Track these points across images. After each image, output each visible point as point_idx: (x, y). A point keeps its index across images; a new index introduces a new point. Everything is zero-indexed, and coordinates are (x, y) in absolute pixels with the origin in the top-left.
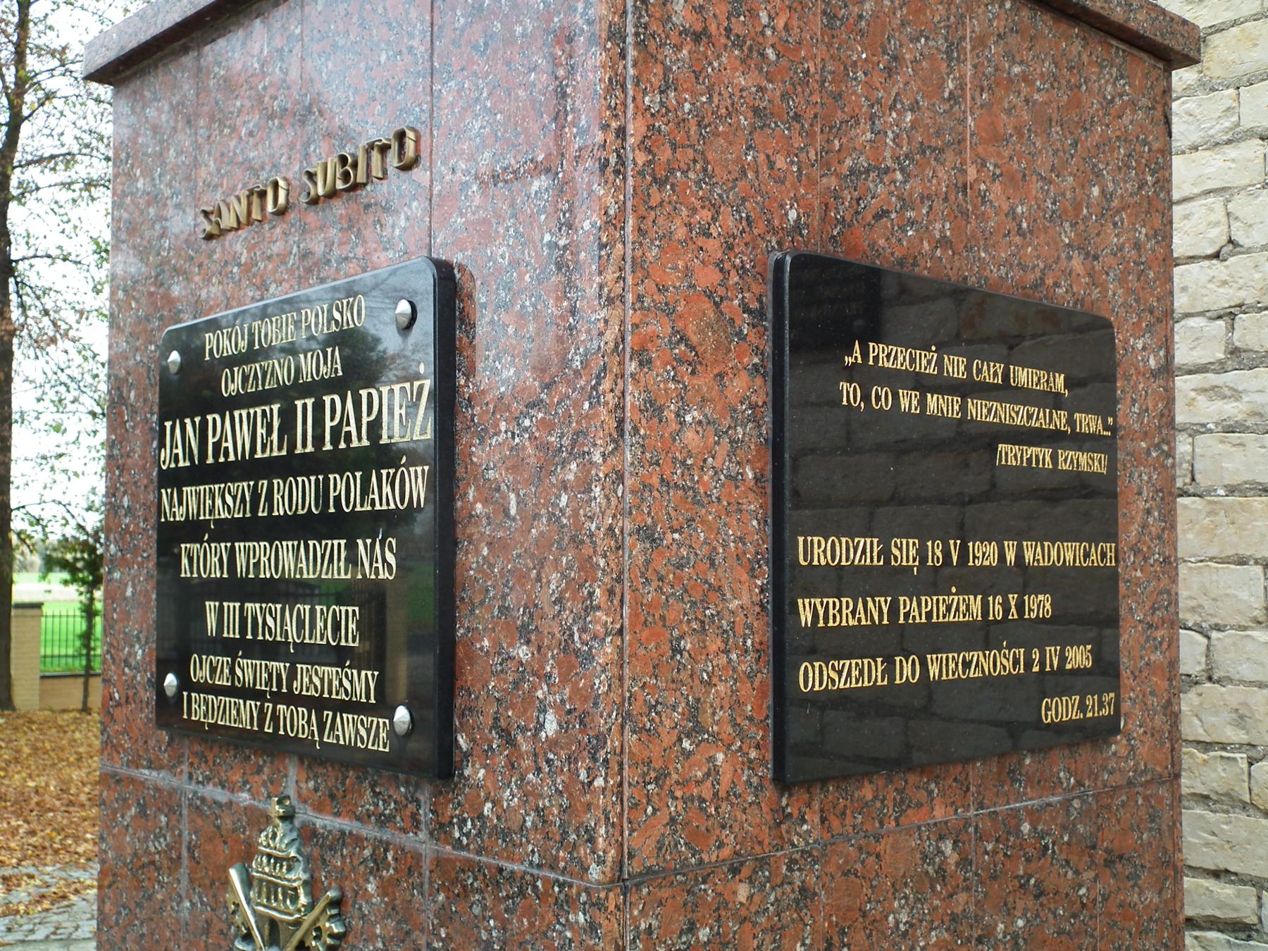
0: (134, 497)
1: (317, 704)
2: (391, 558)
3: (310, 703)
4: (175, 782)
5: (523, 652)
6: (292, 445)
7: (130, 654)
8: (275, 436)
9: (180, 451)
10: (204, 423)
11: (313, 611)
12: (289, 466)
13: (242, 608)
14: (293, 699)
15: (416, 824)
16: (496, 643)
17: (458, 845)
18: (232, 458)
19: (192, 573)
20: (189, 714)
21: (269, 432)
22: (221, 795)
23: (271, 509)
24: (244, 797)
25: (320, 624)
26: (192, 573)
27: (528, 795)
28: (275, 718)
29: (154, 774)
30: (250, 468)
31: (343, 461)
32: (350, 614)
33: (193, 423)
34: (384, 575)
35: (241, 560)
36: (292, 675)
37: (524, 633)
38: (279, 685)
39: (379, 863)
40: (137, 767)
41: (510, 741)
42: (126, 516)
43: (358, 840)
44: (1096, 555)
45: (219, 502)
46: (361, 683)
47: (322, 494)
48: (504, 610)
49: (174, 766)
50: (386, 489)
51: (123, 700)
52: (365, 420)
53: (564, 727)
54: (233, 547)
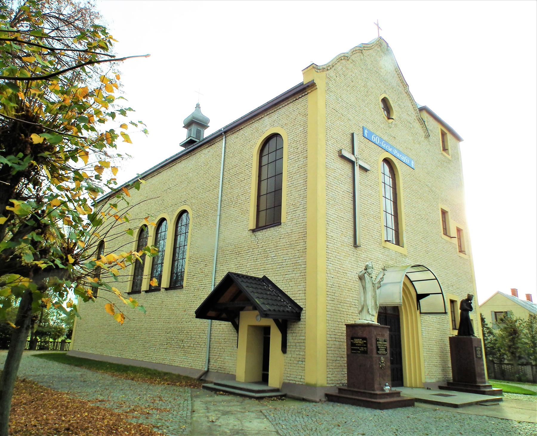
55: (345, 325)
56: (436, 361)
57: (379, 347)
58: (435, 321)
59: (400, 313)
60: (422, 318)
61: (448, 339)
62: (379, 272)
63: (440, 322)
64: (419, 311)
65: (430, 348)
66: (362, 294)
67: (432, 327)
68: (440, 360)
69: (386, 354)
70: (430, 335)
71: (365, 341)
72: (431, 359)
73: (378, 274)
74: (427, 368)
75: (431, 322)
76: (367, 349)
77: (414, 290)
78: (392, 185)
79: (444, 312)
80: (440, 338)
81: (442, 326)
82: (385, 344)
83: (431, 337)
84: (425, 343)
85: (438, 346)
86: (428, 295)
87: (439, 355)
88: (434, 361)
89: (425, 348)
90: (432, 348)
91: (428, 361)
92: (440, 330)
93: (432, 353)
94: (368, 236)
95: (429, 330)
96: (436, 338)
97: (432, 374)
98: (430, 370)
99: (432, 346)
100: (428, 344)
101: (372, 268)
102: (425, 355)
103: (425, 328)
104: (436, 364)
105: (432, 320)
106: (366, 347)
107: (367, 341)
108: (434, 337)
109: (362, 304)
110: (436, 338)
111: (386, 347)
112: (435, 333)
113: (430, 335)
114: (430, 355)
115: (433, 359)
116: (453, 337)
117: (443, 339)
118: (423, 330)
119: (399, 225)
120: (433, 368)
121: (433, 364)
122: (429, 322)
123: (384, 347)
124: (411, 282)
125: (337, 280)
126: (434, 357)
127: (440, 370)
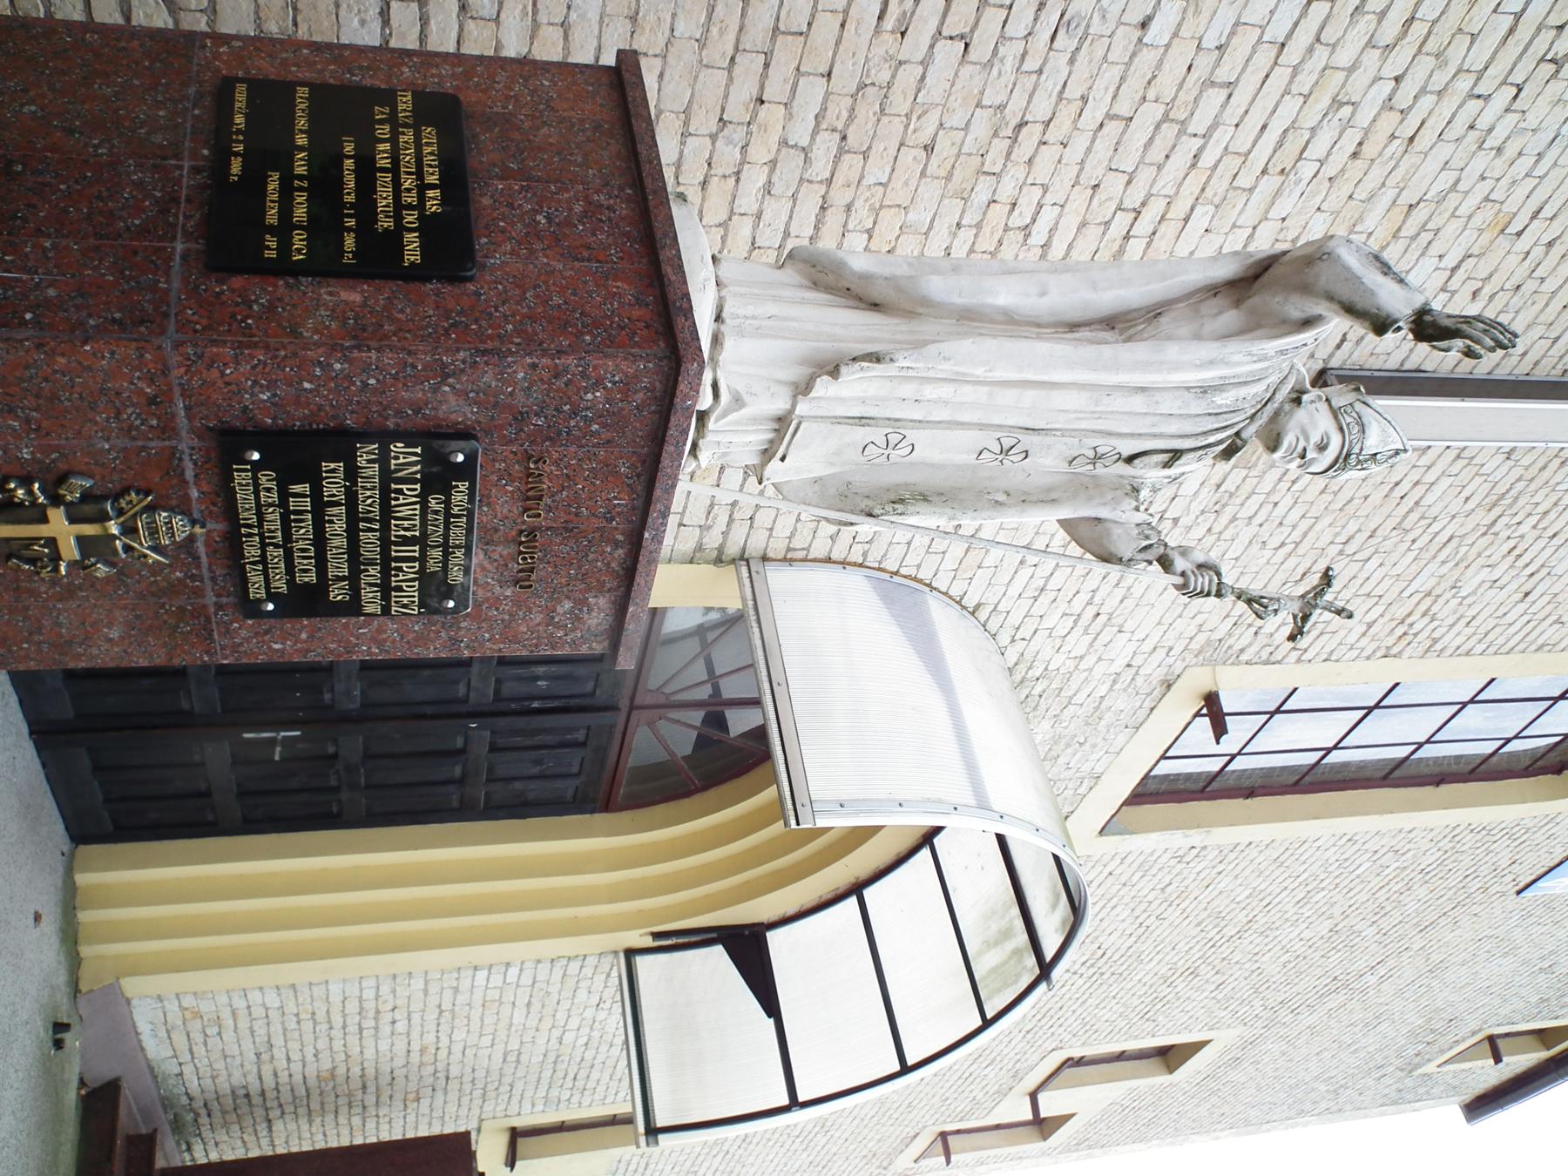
0: (375, 391)
1: (263, 560)
2: (339, 598)
3: (263, 555)
4: (184, 434)
5: (304, 636)
6: (396, 544)
7: (262, 386)
8: (402, 533)
9: (401, 461)
10: (415, 481)
11: (310, 558)
12: (385, 543)
13: (307, 511)
14: (263, 546)
15: (218, 596)
16: (306, 626)
17: (216, 614)
18: (393, 503)
19: (326, 472)
20: (238, 470)
21: (406, 529)
22: (189, 474)
23: (363, 531)
24: (194, 494)
25: (305, 562)
26: (326, 472)
27: (248, 640)
28: (250, 535)
29: (182, 413)
30: (387, 512)
31: (386, 572)
32: (312, 578)
33: (416, 473)
34: (332, 594)
35: (335, 510)
36: (276, 546)
37: (311, 636)
38: (269, 538)
39: (193, 577)
40: (182, 395)
41: (266, 633)
42: (362, 381)
43: (199, 566)
44: (303, 92)
45: (368, 493)
46: (281, 586)
47: (371, 562)
48: (320, 629)
49: (194, 433)
50: (371, 595)
51: (227, 379)
52: (404, 584)
53: (277, 650)
54: (342, 505)
55: (628, 61)
56: (296, 1056)
57: (333, 469)
58: (569, 1038)
59: (626, 816)
60: (591, 961)
61: (462, 1129)
62: (1004, 639)
63: (561, 1067)
64: (649, 942)
65: (387, 1017)
66: (1068, 296)
67: (532, 1022)
68: (311, 1071)
69: (251, 609)
70: (476, 1014)
71: (412, 249)
72: (307, 1026)
73: (993, 625)
74: (240, 1004)
75: (561, 1016)
76: (284, 268)
77: (791, 910)
78: (1345, 765)
79: (660, 1122)
80: (454, 1071)
81: (533, 1078)
82: (386, 589)
83: (460, 1022)
84: (418, 984)
85: (399, 1062)
86: (771, 1006)
87: (341, 1070)
88: (294, 1046)
89: (385, 989)
90: (387, 1029)
91: (291, 1008)
92: (508, 1070)
93: (353, 1028)
94: (1327, 538)
95: (506, 1010)
96: (457, 1048)
97: (197, 1037)
98: (229, 1022)
99: (401, 1027)
100: (416, 1006)
101: (1343, 461)
102: (335, 989)
103: (526, 980)
104: (279, 1054)
105: (574, 1023)
106: (325, 266)
107: (415, 275)
108: (459, 1035)
109: (938, 287)
110: (457, 1048)
111: (353, 607)
112: (486, 1041)
113: (476, 1014)
114: (337, 1020)
115: (308, 1038)
116: (471, 1156)
117: (454, 1085)
118: (513, 973)
119: (1428, 791)
120: (247, 1045)
121: (278, 1041)
122: (566, 1005)
123: (338, 566)
124: (857, 889)
125: (1094, 114)
126: (322, 1044)
127: (237, 1079)
